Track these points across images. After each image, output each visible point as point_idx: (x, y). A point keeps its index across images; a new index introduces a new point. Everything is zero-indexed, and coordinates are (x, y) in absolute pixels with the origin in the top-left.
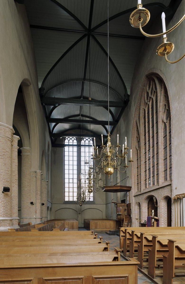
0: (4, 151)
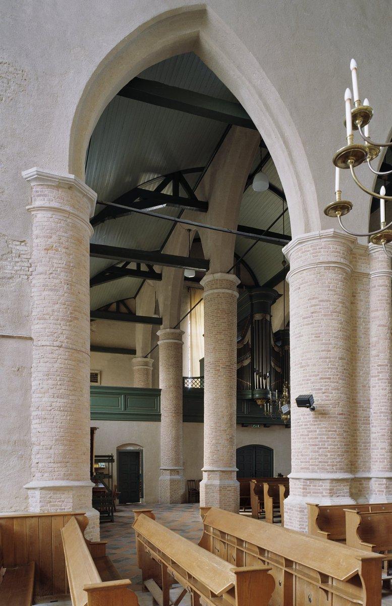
0: (314, 302)
